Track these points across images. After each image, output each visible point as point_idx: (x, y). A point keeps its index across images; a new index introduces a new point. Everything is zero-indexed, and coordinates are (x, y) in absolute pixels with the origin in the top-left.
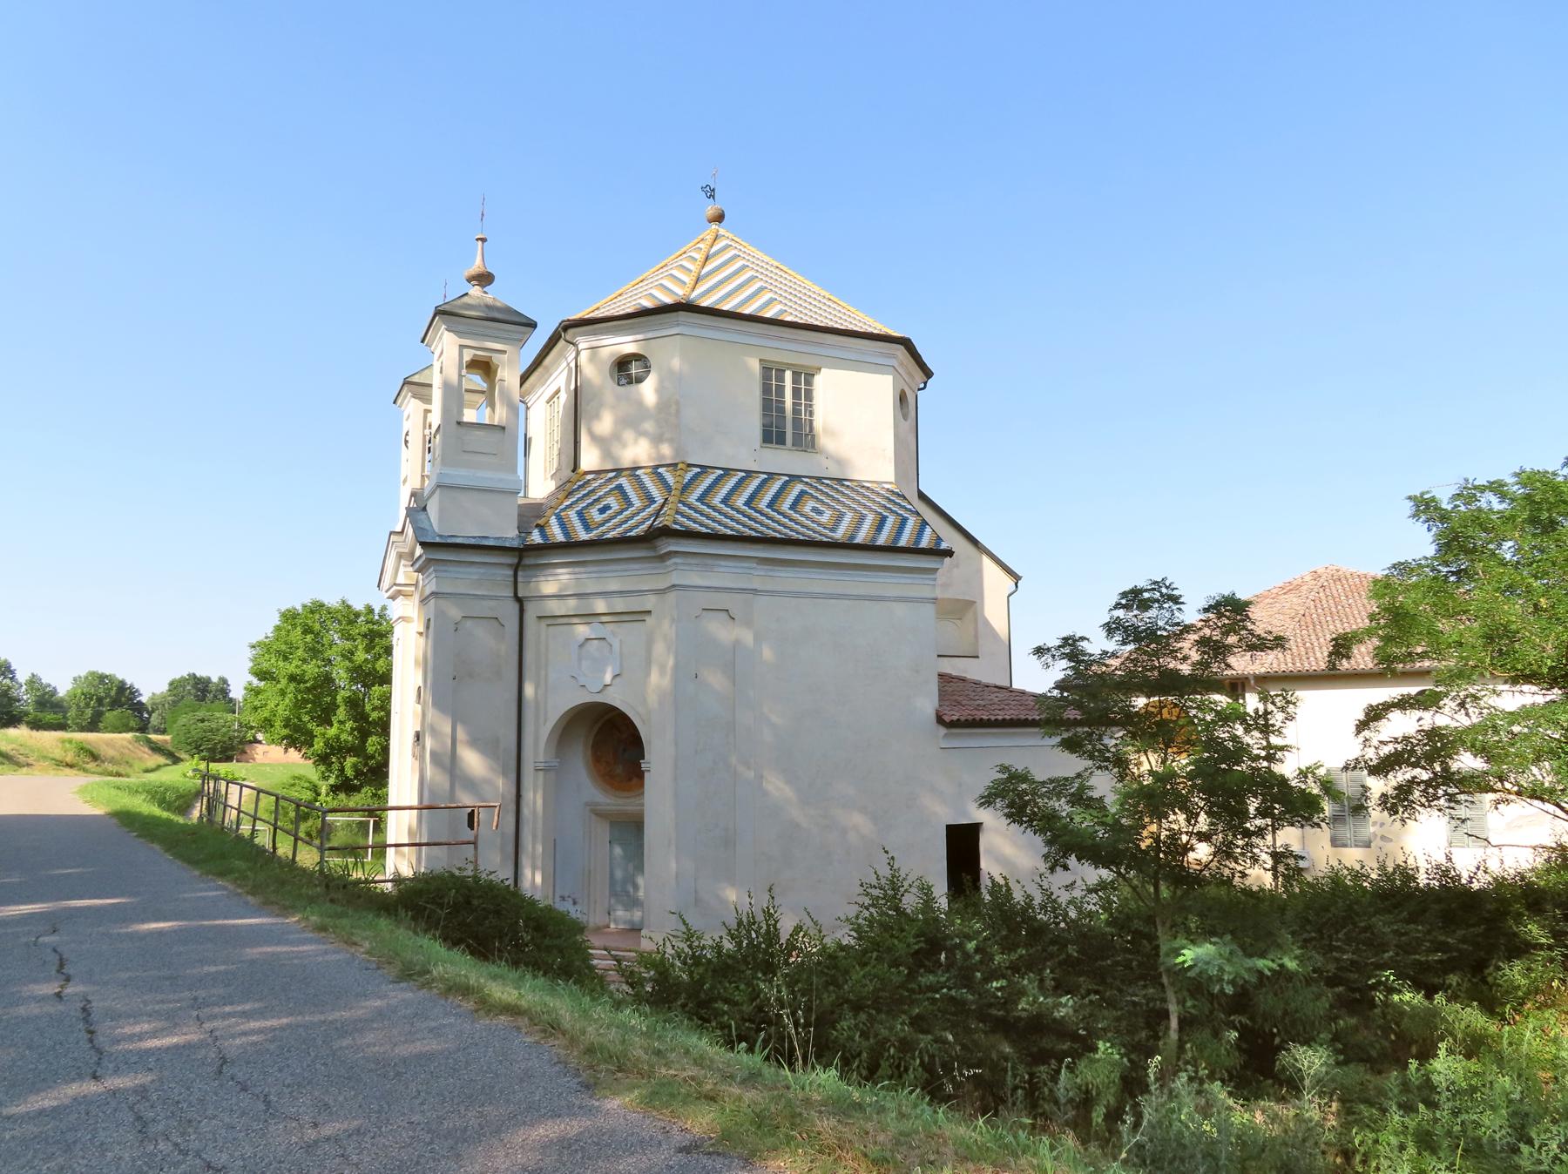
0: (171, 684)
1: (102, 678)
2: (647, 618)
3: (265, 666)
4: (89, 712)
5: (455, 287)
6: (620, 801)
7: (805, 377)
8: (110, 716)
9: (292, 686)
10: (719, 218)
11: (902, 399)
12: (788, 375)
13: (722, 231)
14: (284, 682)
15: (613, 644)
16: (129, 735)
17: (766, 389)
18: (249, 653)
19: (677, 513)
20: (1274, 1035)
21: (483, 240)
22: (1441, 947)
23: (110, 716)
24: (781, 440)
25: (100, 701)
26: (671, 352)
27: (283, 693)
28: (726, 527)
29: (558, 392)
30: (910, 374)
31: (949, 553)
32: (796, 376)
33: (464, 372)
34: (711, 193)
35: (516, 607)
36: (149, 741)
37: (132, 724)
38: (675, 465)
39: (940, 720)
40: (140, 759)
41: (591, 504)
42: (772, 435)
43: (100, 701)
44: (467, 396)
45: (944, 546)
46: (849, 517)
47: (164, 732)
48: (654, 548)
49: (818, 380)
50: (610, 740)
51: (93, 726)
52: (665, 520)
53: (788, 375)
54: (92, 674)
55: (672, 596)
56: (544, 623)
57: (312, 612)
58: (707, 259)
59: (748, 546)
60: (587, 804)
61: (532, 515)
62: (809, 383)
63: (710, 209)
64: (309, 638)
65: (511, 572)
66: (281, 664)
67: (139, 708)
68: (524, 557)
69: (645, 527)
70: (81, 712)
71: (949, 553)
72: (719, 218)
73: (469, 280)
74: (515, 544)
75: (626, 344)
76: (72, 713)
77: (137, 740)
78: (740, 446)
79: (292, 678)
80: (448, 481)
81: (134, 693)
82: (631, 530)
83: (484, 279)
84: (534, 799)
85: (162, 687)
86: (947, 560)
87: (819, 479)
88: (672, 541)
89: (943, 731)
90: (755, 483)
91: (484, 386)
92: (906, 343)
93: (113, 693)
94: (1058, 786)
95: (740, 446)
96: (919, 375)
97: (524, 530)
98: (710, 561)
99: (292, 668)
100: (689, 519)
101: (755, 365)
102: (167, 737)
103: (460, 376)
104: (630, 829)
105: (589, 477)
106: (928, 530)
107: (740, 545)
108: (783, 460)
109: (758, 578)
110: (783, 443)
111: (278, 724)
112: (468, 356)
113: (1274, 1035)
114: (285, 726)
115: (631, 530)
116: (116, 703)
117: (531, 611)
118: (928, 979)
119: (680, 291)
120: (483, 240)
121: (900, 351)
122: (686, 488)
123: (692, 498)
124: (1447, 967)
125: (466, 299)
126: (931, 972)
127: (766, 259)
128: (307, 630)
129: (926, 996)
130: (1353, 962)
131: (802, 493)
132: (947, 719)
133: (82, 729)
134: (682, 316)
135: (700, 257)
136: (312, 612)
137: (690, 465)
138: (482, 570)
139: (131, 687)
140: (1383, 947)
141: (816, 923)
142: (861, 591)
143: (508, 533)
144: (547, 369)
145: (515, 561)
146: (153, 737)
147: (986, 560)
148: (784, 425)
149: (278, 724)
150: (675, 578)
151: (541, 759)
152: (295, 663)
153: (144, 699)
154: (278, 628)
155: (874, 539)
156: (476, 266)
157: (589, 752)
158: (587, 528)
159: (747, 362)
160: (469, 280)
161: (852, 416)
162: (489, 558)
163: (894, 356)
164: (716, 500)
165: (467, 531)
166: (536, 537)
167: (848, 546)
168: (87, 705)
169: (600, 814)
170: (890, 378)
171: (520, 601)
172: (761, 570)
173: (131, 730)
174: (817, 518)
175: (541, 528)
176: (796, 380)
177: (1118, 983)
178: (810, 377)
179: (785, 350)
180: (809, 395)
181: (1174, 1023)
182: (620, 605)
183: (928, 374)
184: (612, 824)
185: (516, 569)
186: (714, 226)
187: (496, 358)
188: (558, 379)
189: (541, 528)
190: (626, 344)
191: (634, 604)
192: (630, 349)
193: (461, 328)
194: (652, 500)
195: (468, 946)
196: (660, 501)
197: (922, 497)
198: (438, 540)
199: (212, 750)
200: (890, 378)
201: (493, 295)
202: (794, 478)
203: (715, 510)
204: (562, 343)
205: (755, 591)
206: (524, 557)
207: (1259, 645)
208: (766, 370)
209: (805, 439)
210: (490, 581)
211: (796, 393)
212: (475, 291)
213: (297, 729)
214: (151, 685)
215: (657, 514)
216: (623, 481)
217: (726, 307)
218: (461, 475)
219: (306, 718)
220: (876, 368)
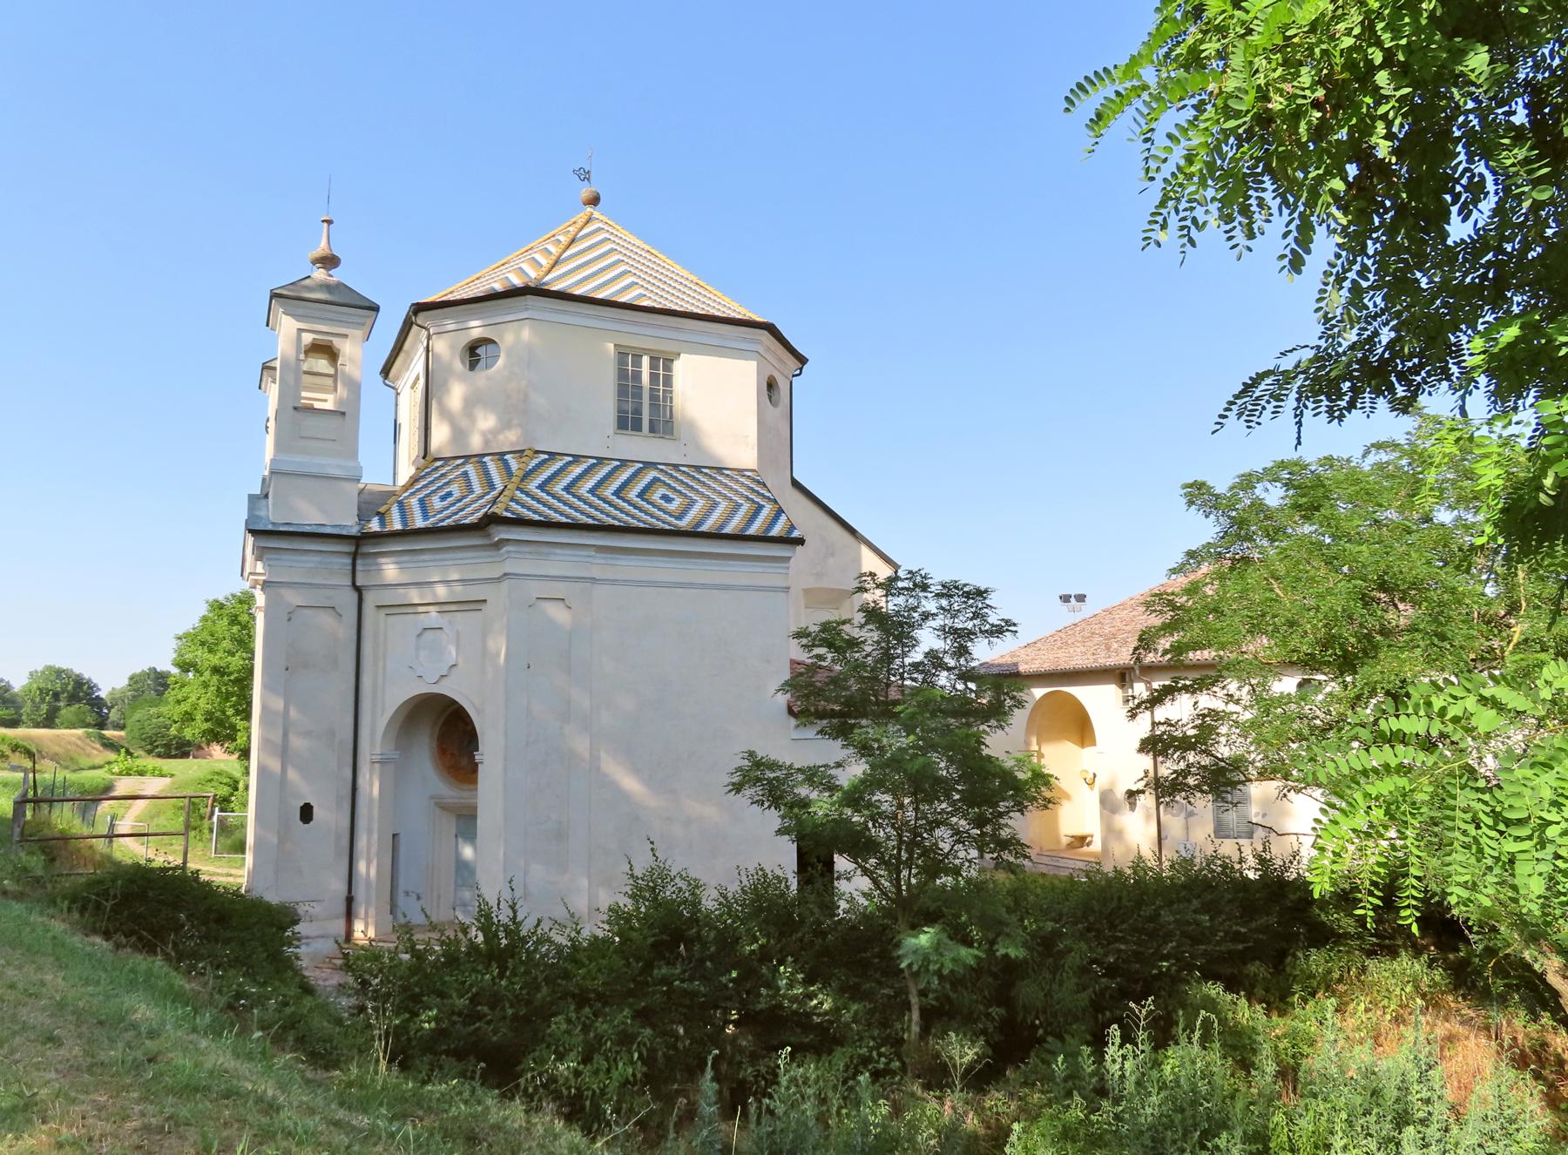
0: (131, 678)
1: (59, 673)
2: (483, 607)
3: (189, 657)
4: (44, 708)
5: (297, 268)
6: (465, 794)
7: (663, 363)
8: (67, 712)
9: (216, 678)
10: (594, 201)
11: (771, 385)
12: (646, 360)
13: (596, 214)
14: (207, 674)
15: (444, 631)
16: (80, 732)
17: (622, 374)
18: (174, 644)
19: (512, 500)
20: (1037, 1028)
21: (329, 222)
22: (1237, 937)
23: (67, 712)
24: (637, 427)
25: (56, 696)
26: (517, 333)
27: (206, 685)
28: (633, 517)
29: (417, 378)
30: (780, 360)
31: (792, 541)
32: (654, 361)
33: (302, 356)
34: (585, 176)
35: (355, 596)
36: (102, 737)
37: (89, 719)
38: (522, 451)
39: (791, 712)
40: (88, 755)
41: (434, 492)
42: (628, 422)
43: (56, 696)
44: (307, 379)
45: (795, 534)
46: (723, 506)
47: (122, 728)
48: (489, 536)
49: (679, 367)
50: (447, 730)
51: (49, 721)
52: (498, 509)
53: (646, 360)
54: (49, 668)
55: (505, 584)
56: (383, 612)
57: (241, 602)
58: (573, 241)
59: (585, 533)
60: (432, 797)
61: (372, 504)
62: (668, 368)
63: (585, 191)
64: (235, 629)
65: (349, 561)
66: (207, 655)
67: (97, 703)
68: (360, 545)
69: (480, 514)
70: (37, 708)
71: (792, 541)
72: (594, 201)
73: (315, 262)
74: (354, 531)
75: (476, 328)
76: (27, 709)
77: (89, 735)
78: (591, 429)
79: (216, 670)
80: (285, 468)
81: (92, 687)
82: (465, 517)
83: (329, 261)
84: (371, 786)
85: (121, 682)
86: (799, 548)
87: (698, 468)
88: (500, 528)
89: (793, 722)
90: (606, 469)
91: (332, 371)
92: (770, 328)
93: (70, 688)
94: (812, 775)
95: (591, 429)
96: (793, 363)
97: (363, 517)
98: (545, 549)
99: (215, 660)
100: (523, 506)
101: (611, 346)
102: (122, 733)
103: (298, 360)
104: (466, 821)
105: (438, 463)
106: (783, 518)
107: (577, 533)
108: (639, 447)
109: (598, 567)
110: (640, 430)
111: (199, 717)
112: (308, 338)
113: (1037, 1028)
114: (206, 720)
115: (465, 517)
116: (73, 698)
117: (370, 599)
118: (662, 971)
119: (533, 274)
120: (329, 222)
121: (765, 336)
122: (527, 475)
123: (532, 486)
124: (1245, 957)
125: (307, 282)
126: (668, 964)
127: (638, 242)
128: (234, 620)
129: (680, 990)
130: (1136, 953)
131: (655, 480)
132: (796, 709)
133: (37, 725)
134: (531, 300)
135: (564, 239)
136: (241, 602)
137: (537, 452)
138: (317, 558)
139: (89, 681)
140: (1168, 937)
141: (572, 916)
142: (744, 581)
143: (348, 522)
144: (408, 353)
145: (352, 549)
146: (107, 733)
147: (865, 550)
148: (643, 407)
149: (199, 717)
150: (510, 567)
151: (378, 750)
152: (219, 655)
153: (103, 694)
154: (204, 619)
155: (722, 526)
156: (321, 248)
157: (434, 745)
158: (425, 516)
159: (599, 347)
160: (315, 262)
161: (716, 398)
162: (331, 545)
163: (760, 343)
164: (632, 495)
165: (310, 515)
166: (374, 526)
167: (693, 534)
168: (43, 700)
169: (444, 807)
170: (754, 364)
171: (359, 590)
172: (600, 559)
173: (88, 726)
174: (667, 508)
175: (382, 516)
176: (654, 366)
177: (878, 975)
178: (668, 362)
179: (643, 335)
180: (668, 381)
181: (916, 1015)
182: (461, 592)
183: (803, 360)
184: (459, 816)
185: (355, 556)
186: (589, 209)
187: (336, 342)
188: (413, 369)
189: (382, 516)
190: (476, 328)
191: (475, 593)
192: (476, 333)
193: (300, 311)
194: (492, 486)
195: (140, 938)
196: (500, 487)
197: (796, 484)
198: (270, 527)
199: (167, 746)
200: (754, 364)
201: (337, 275)
202: (649, 465)
203: (654, 506)
204: (415, 328)
205: (593, 580)
206: (360, 545)
207: (998, 631)
208: (622, 355)
209: (663, 423)
210: (332, 568)
211: (654, 377)
212: (319, 274)
213: (220, 723)
214: (109, 681)
215: (494, 501)
216: (470, 468)
217: (578, 292)
218: (297, 461)
219: (230, 712)
220: (740, 353)
